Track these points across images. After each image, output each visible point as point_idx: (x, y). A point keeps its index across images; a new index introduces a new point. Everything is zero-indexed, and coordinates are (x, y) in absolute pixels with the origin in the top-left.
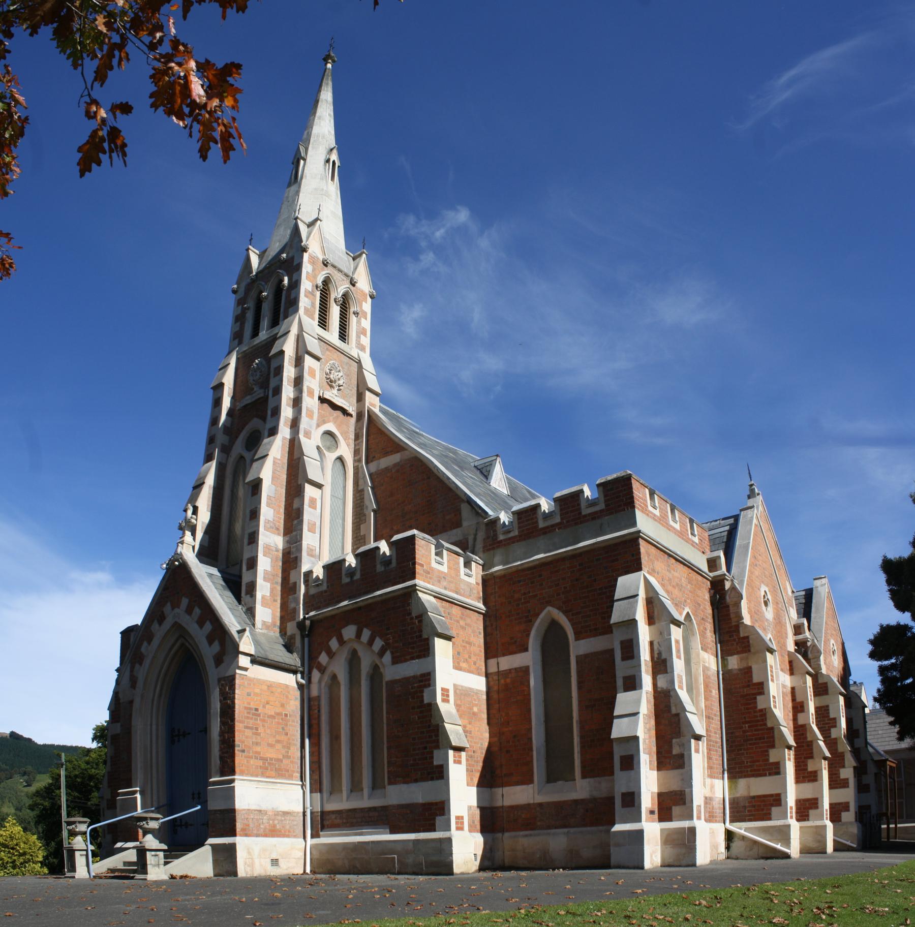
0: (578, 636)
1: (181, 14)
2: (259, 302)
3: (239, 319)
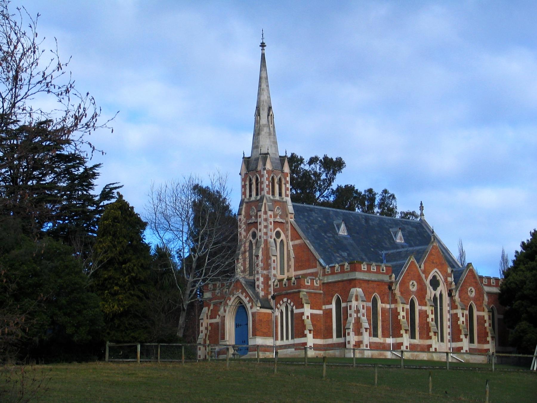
2: (250, 180)
3: (244, 186)
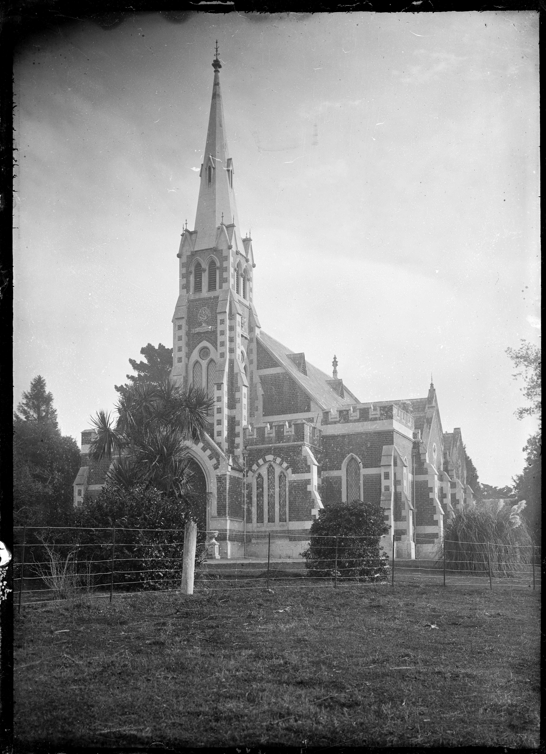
0: (365, 466)
1: (437, 392)
3: (184, 276)
